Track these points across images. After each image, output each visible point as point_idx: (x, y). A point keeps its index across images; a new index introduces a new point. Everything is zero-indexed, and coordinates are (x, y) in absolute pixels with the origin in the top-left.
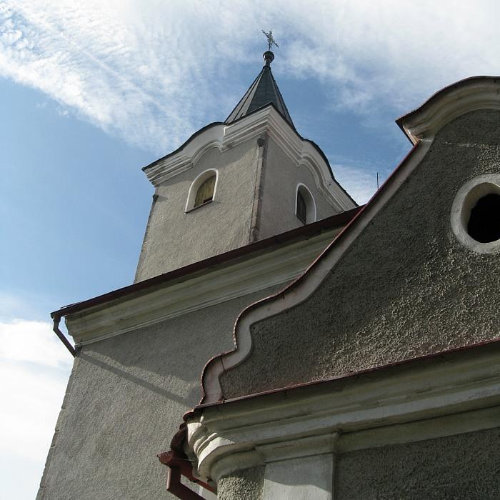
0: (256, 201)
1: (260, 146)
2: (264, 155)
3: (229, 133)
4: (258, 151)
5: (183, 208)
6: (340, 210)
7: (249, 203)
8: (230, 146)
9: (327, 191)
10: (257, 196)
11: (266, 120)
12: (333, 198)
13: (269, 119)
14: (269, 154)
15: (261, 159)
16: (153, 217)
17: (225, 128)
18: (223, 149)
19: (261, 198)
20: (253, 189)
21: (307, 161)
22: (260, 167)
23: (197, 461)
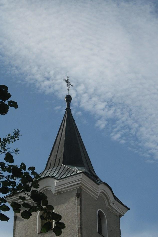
0: (80, 235)
1: (77, 197)
2: (80, 204)
3: (58, 184)
4: (77, 200)
5: (35, 229)
6: (119, 214)
7: (76, 235)
8: (59, 193)
9: (112, 207)
10: (79, 231)
11: (81, 179)
12: (115, 209)
13: (82, 181)
14: (83, 201)
15: (79, 207)
16: (16, 231)
17: (56, 181)
18: (55, 194)
19: (82, 232)
20: (77, 226)
21: (102, 194)
22: (79, 212)
23: (12, 204)
